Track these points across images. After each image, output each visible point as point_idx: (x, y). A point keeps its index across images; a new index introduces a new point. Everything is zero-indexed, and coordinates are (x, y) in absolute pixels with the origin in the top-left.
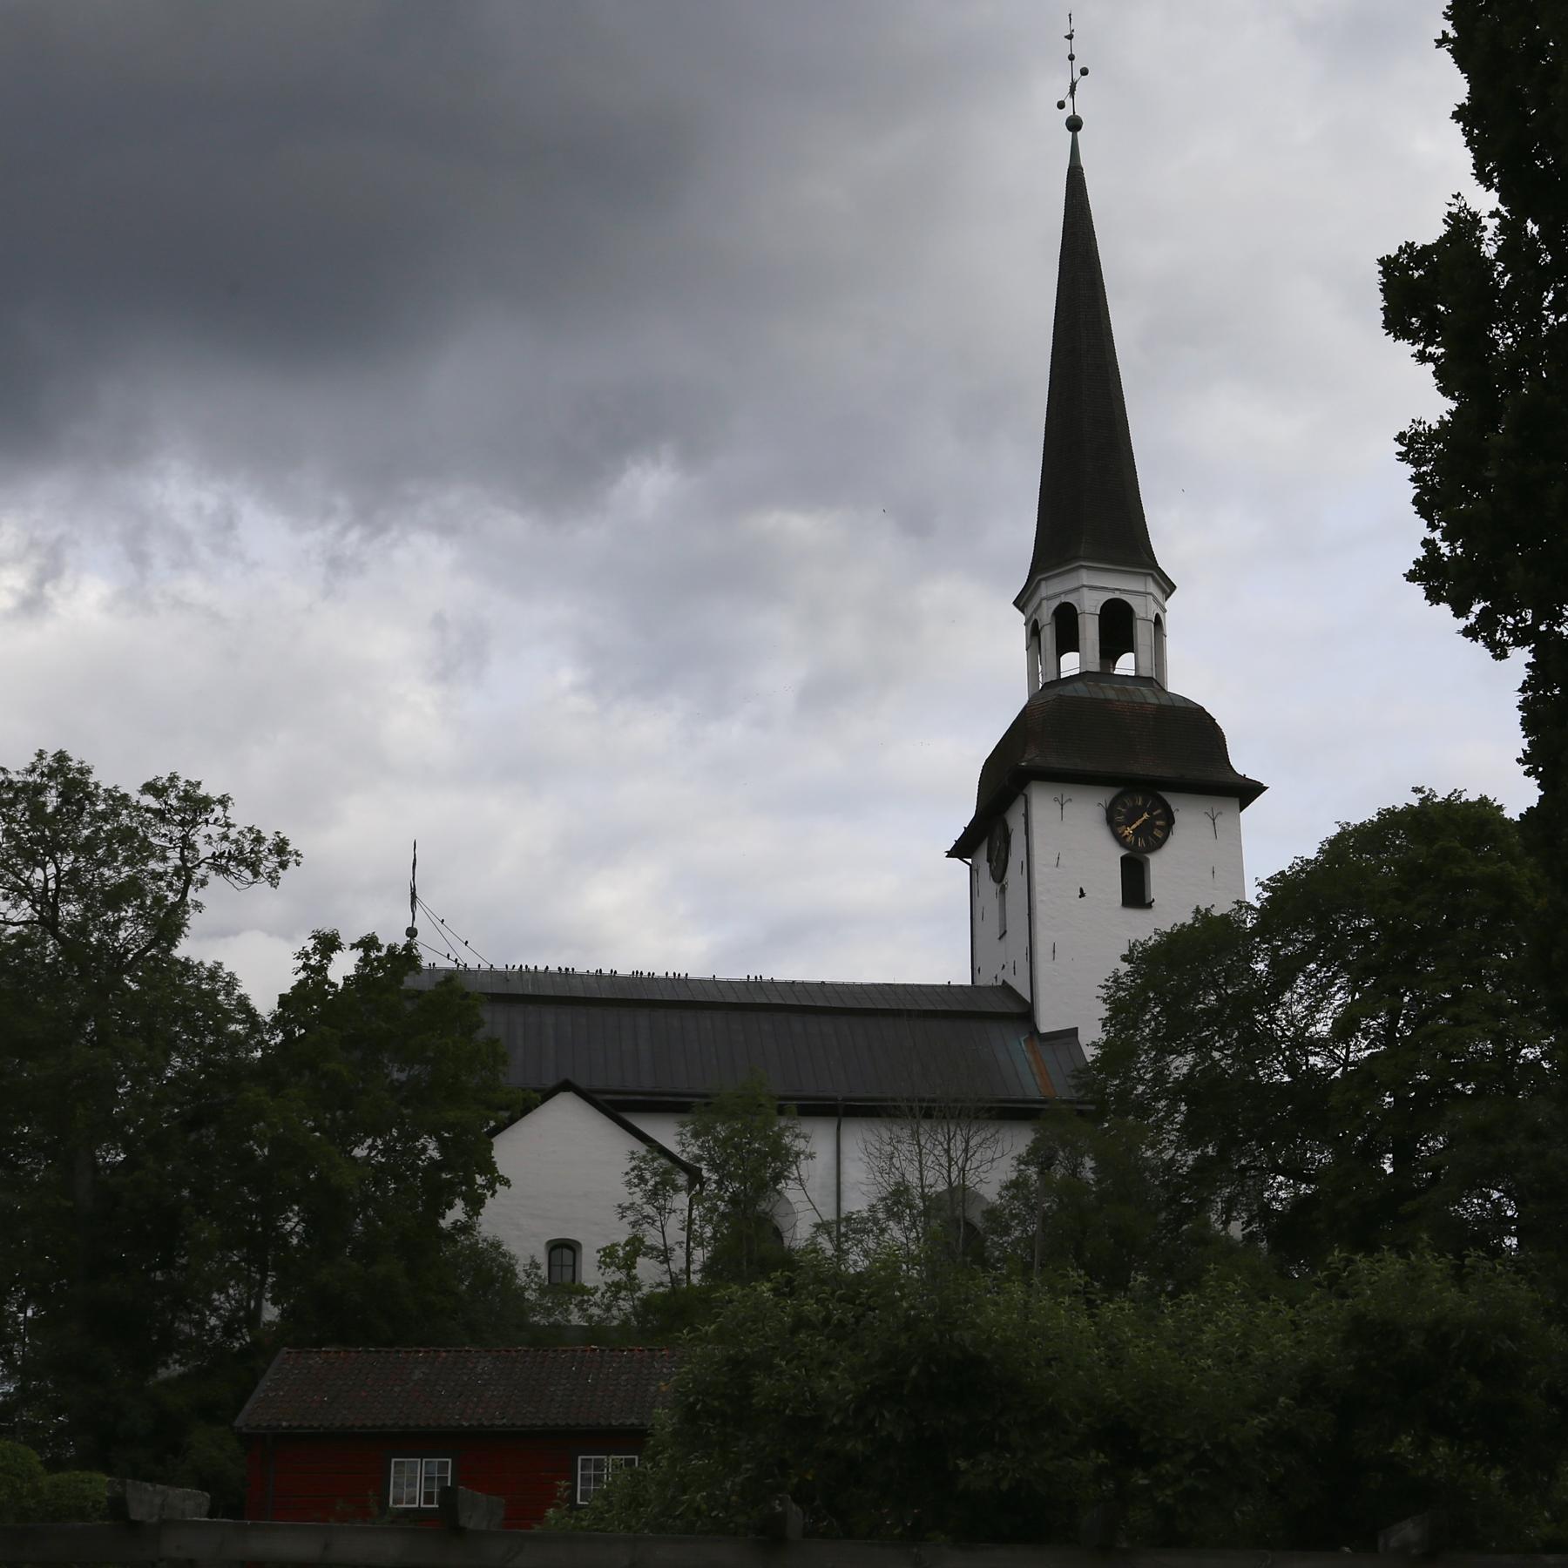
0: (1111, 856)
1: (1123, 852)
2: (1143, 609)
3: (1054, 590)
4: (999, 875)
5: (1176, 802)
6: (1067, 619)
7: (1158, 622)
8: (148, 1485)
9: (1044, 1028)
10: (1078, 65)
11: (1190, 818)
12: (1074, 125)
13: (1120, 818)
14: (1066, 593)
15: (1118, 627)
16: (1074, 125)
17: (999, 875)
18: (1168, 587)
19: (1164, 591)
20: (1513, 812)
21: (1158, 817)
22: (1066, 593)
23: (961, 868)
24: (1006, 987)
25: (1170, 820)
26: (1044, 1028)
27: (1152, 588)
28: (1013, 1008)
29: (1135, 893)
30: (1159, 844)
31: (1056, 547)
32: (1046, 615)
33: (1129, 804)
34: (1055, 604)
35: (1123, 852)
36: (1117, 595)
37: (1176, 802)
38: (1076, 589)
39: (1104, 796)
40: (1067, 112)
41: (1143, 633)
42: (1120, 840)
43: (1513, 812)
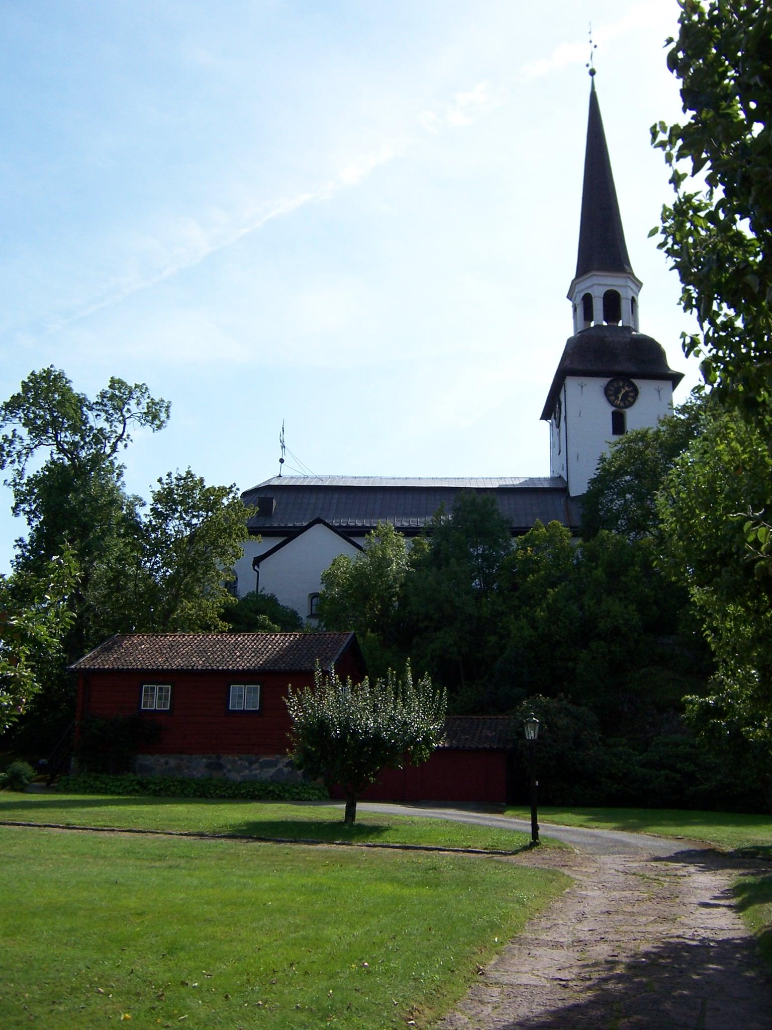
0: (607, 410)
1: (613, 409)
2: (625, 295)
3: (586, 285)
4: (558, 426)
5: (637, 382)
6: (587, 300)
7: (634, 301)
8: (149, 757)
9: (572, 495)
10: (593, 44)
11: (645, 388)
12: (592, 73)
13: (611, 393)
14: (587, 288)
15: (612, 303)
16: (592, 73)
17: (558, 426)
18: (639, 285)
19: (637, 286)
20: (723, 187)
21: (631, 391)
22: (587, 288)
23: (546, 424)
24: (560, 477)
25: (636, 392)
26: (572, 495)
27: (630, 284)
28: (561, 486)
29: (618, 425)
30: (631, 404)
31: (584, 267)
32: (579, 300)
33: (616, 385)
34: (582, 295)
35: (613, 409)
36: (612, 288)
37: (637, 382)
38: (592, 286)
39: (604, 381)
40: (590, 68)
41: (625, 306)
42: (612, 403)
43: (723, 187)
